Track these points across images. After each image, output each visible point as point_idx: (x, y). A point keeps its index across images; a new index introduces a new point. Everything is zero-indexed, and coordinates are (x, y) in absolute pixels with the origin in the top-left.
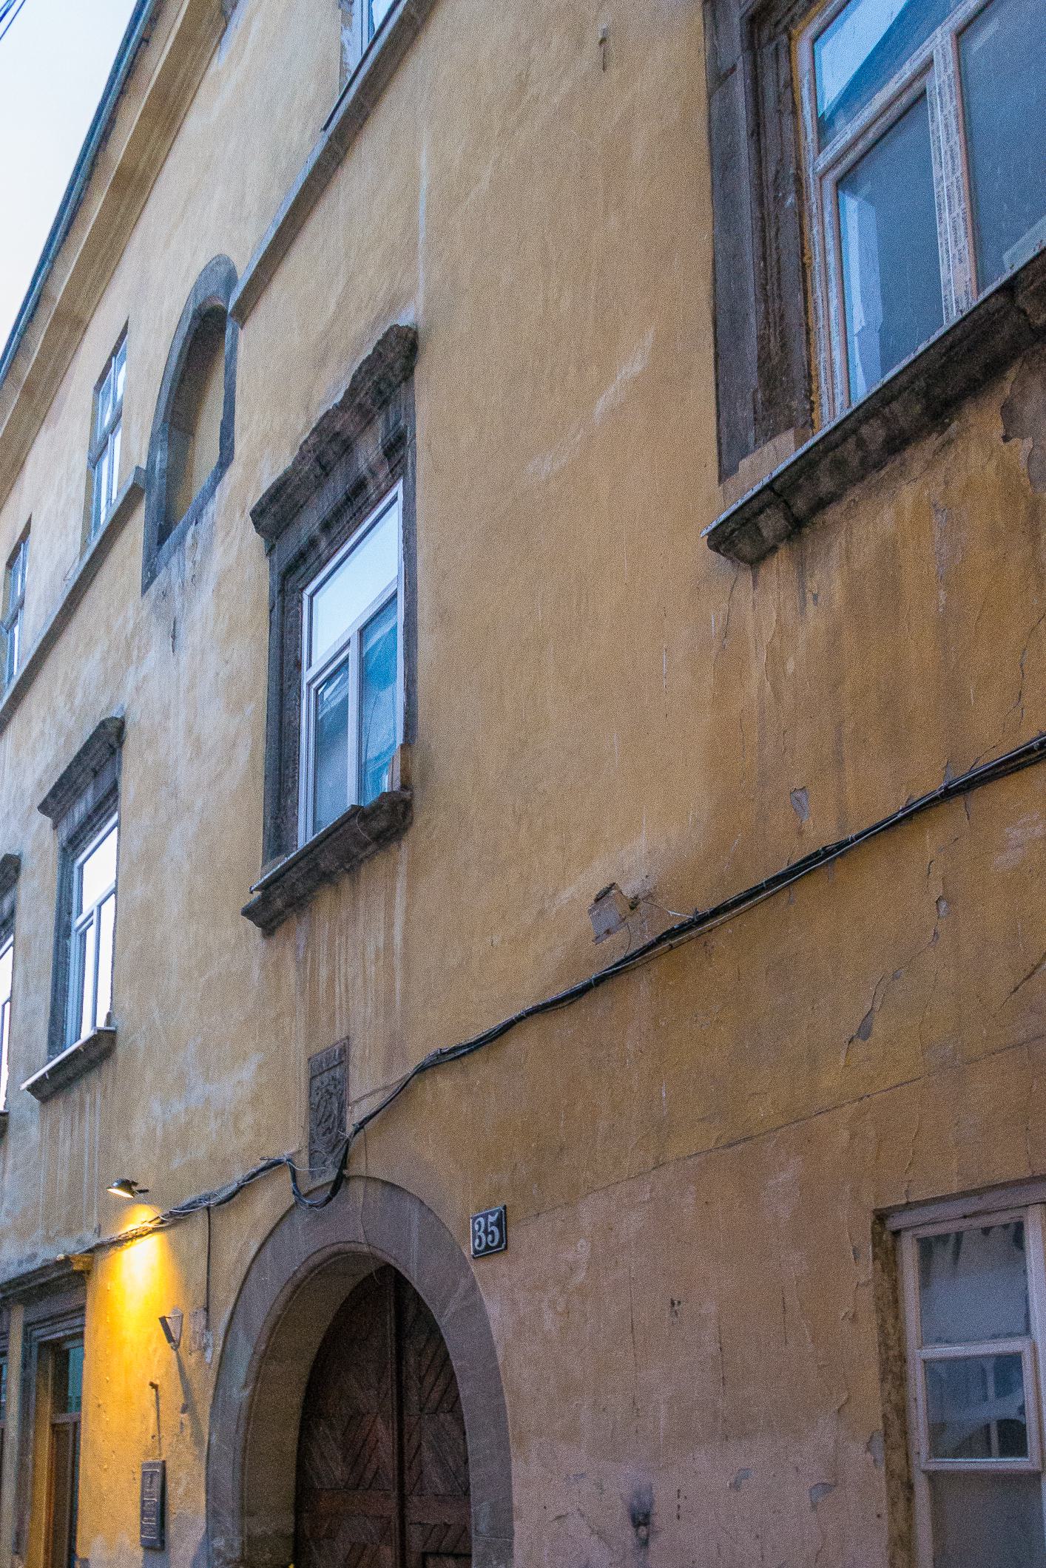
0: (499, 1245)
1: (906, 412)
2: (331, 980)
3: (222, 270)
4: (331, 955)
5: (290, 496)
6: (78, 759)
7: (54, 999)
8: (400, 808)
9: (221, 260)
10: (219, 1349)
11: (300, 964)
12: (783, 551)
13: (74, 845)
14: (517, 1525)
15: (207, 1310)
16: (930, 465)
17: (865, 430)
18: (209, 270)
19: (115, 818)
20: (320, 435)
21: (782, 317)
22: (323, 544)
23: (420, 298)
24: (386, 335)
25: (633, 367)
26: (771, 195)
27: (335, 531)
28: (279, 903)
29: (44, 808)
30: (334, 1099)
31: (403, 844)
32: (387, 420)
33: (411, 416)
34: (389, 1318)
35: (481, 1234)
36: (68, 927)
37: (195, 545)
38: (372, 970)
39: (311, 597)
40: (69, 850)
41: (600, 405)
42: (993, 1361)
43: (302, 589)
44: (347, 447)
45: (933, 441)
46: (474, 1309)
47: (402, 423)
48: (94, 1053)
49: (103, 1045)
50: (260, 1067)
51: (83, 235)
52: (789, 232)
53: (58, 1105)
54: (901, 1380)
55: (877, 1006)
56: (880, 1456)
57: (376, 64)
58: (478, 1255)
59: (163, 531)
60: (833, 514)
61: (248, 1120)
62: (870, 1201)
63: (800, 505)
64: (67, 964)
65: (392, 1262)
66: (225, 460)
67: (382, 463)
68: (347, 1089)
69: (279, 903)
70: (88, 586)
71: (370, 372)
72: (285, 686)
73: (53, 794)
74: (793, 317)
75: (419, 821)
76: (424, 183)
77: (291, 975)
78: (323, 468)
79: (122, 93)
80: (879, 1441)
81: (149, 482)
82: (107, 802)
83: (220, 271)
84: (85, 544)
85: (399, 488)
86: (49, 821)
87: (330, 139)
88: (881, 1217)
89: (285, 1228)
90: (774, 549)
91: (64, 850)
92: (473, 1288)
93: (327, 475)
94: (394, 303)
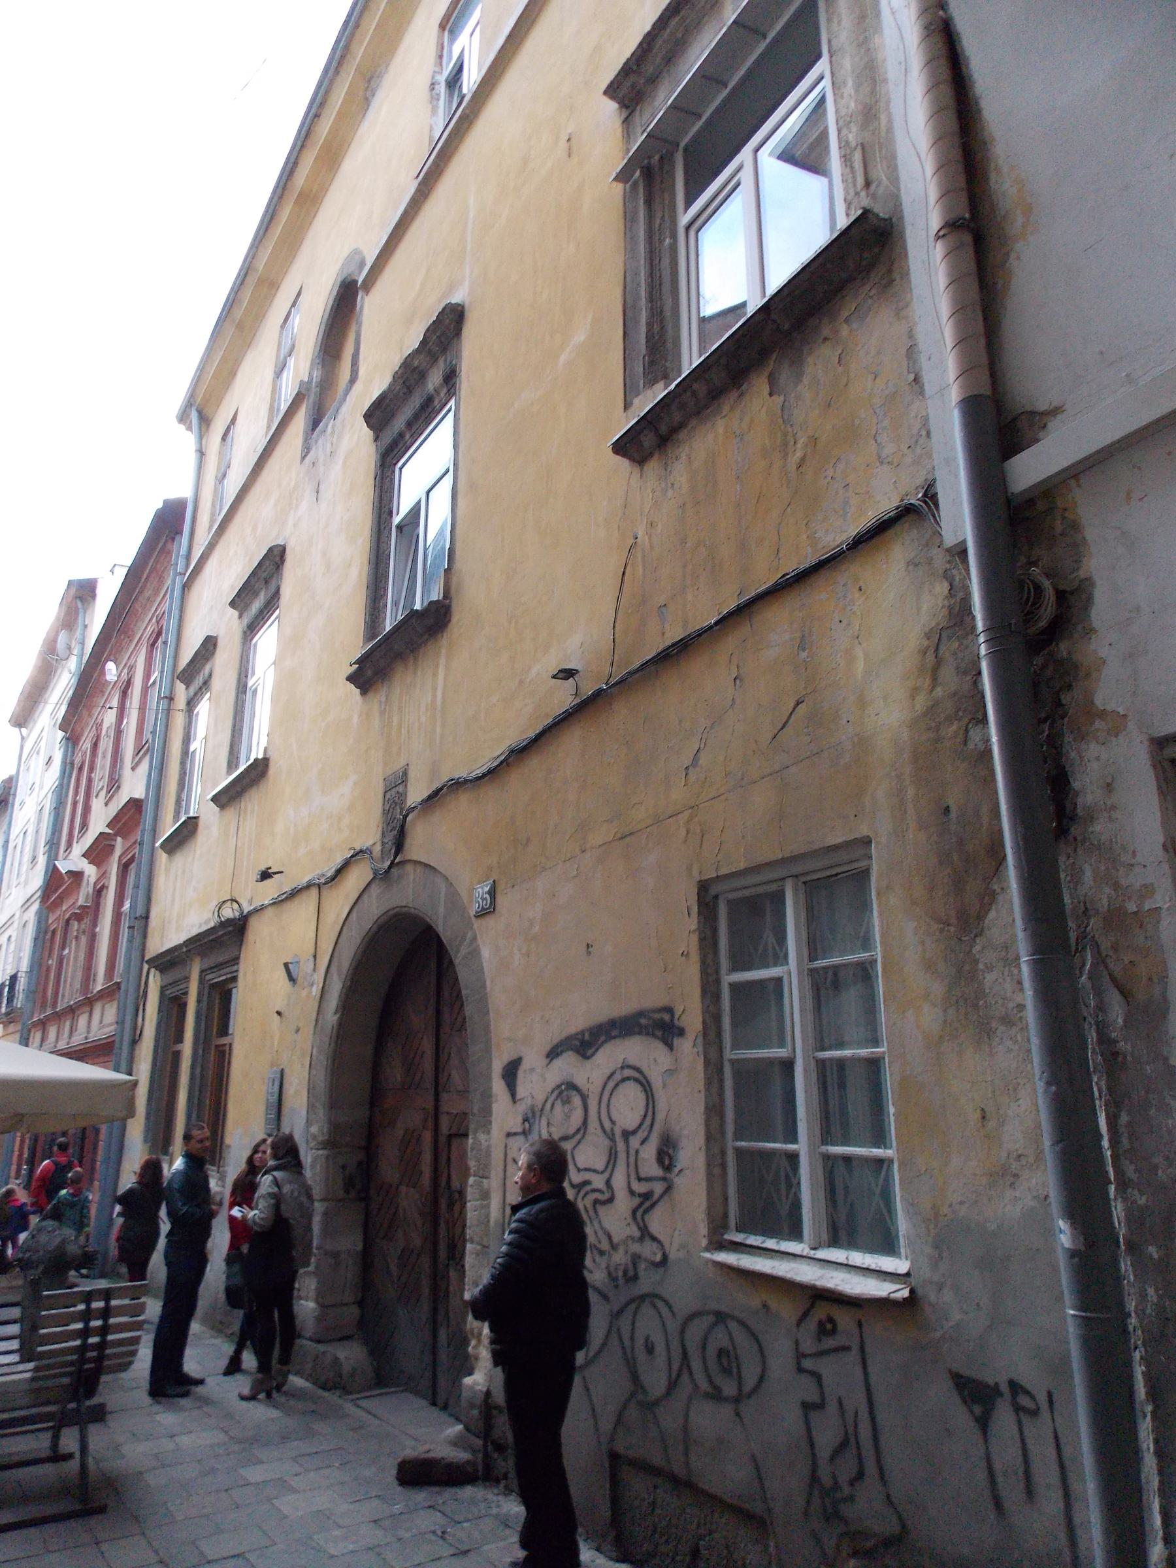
0: (490, 907)
1: (717, 376)
2: (400, 726)
3: (357, 257)
4: (400, 708)
5: (388, 405)
6: (254, 573)
7: (233, 736)
8: (443, 610)
9: (357, 252)
10: (321, 985)
11: (382, 713)
12: (656, 457)
13: (252, 629)
14: (495, 1106)
15: (315, 957)
16: (732, 408)
17: (696, 386)
18: (349, 259)
19: (277, 612)
20: (405, 367)
21: (661, 312)
22: (407, 436)
23: (467, 283)
24: (444, 309)
25: (580, 337)
26: (657, 238)
27: (414, 429)
28: (369, 673)
29: (233, 604)
30: (398, 807)
31: (445, 635)
32: (446, 360)
33: (458, 356)
34: (433, 965)
35: (479, 899)
36: (245, 686)
37: (333, 433)
38: (423, 719)
39: (401, 469)
40: (248, 633)
41: (563, 358)
42: (773, 982)
43: (395, 464)
44: (422, 376)
45: (734, 395)
46: (475, 953)
47: (454, 362)
48: (253, 774)
49: (259, 770)
50: (355, 784)
51: (277, 230)
52: (666, 262)
53: (231, 813)
54: (717, 997)
55: (702, 746)
56: (701, 1049)
57: (447, 141)
58: (478, 916)
59: (315, 422)
60: (682, 435)
61: (346, 821)
62: (697, 877)
63: (663, 429)
64: (243, 712)
65: (428, 920)
66: (353, 380)
67: (441, 385)
68: (405, 798)
69: (369, 673)
70: (269, 456)
71: (434, 331)
72: (382, 527)
73: (238, 595)
74: (668, 313)
75: (455, 618)
76: (471, 215)
77: (376, 722)
78: (408, 388)
79: (302, 147)
80: (700, 1040)
81: (308, 390)
82: (272, 603)
83: (356, 257)
84: (269, 427)
85: (452, 403)
86: (236, 613)
87: (419, 184)
88: (704, 887)
89: (365, 896)
90: (651, 455)
91: (245, 633)
92: (475, 939)
93: (411, 392)
94: (452, 287)
